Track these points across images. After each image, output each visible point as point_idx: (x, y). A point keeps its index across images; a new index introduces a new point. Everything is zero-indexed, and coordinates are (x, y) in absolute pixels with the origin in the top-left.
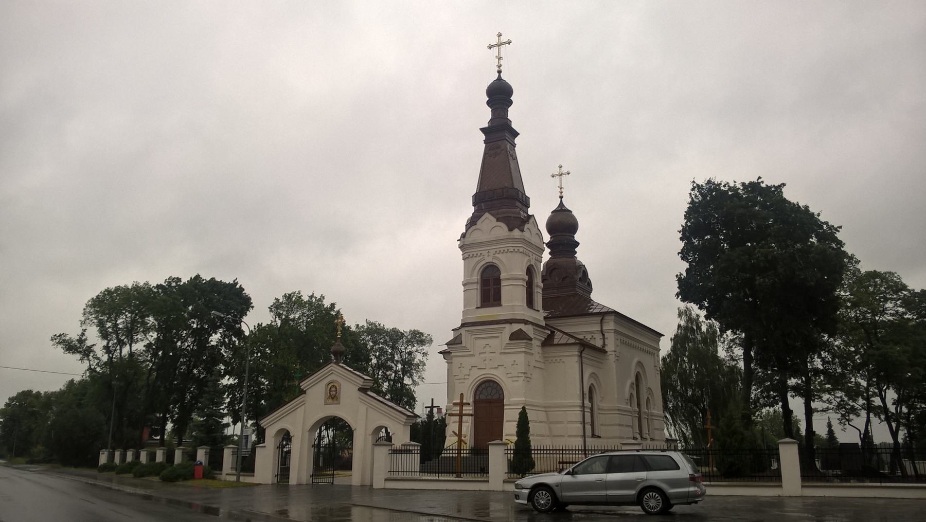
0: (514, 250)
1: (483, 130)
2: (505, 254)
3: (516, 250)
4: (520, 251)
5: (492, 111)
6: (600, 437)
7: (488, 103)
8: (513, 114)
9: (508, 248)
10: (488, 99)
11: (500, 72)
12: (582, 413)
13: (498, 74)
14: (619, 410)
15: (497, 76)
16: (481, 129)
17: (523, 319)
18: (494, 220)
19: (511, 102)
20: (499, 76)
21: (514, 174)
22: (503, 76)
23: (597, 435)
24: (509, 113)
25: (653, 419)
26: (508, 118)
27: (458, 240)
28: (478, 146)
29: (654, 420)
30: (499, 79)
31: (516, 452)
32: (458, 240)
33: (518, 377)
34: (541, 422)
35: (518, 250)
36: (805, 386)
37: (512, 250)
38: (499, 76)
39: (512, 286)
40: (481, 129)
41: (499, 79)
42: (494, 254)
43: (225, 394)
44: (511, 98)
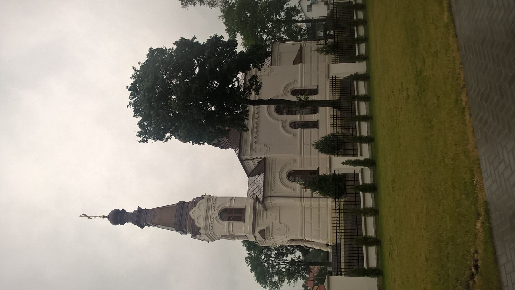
0: (213, 206)
1: (139, 208)
2: (216, 204)
3: (214, 207)
4: (215, 200)
5: (127, 222)
6: (318, 167)
7: (122, 224)
8: (131, 209)
9: (211, 230)
10: (120, 224)
11: (104, 217)
12: (305, 198)
13: (105, 218)
14: (301, 154)
15: (106, 218)
16: (138, 207)
17: (252, 229)
18: (195, 208)
19: (123, 210)
20: (106, 217)
21: (165, 227)
22: (107, 214)
23: (316, 88)
24: (130, 212)
25: (304, 86)
26: (132, 212)
27: (209, 243)
28: (150, 230)
29: (305, 85)
30: (108, 217)
31: (331, 12)
32: (209, 243)
33: (286, 228)
34: (311, 212)
35: (214, 201)
36: (276, 261)
37: (212, 225)
38: (106, 217)
39: (233, 229)
40: (138, 207)
41: (108, 217)
42: (214, 210)
43: (322, 266)
44: (121, 210)
